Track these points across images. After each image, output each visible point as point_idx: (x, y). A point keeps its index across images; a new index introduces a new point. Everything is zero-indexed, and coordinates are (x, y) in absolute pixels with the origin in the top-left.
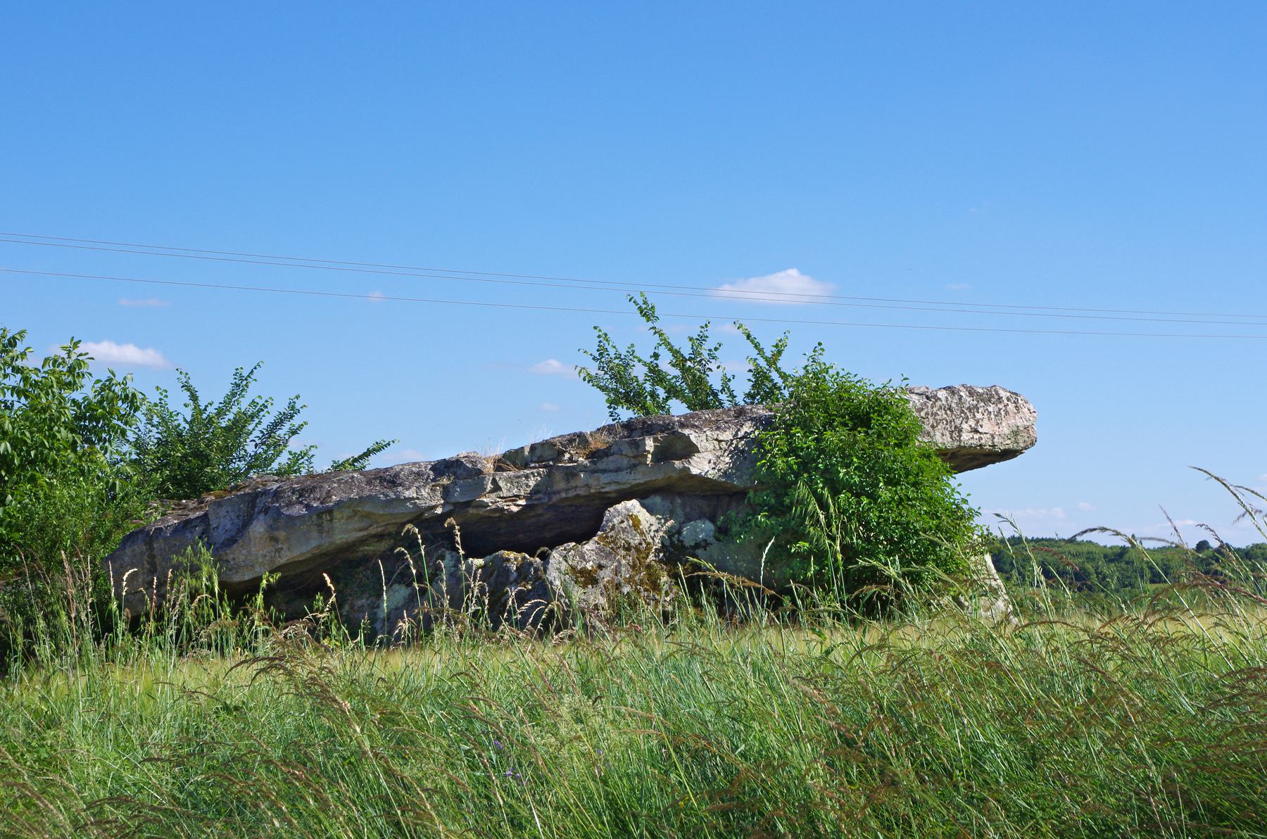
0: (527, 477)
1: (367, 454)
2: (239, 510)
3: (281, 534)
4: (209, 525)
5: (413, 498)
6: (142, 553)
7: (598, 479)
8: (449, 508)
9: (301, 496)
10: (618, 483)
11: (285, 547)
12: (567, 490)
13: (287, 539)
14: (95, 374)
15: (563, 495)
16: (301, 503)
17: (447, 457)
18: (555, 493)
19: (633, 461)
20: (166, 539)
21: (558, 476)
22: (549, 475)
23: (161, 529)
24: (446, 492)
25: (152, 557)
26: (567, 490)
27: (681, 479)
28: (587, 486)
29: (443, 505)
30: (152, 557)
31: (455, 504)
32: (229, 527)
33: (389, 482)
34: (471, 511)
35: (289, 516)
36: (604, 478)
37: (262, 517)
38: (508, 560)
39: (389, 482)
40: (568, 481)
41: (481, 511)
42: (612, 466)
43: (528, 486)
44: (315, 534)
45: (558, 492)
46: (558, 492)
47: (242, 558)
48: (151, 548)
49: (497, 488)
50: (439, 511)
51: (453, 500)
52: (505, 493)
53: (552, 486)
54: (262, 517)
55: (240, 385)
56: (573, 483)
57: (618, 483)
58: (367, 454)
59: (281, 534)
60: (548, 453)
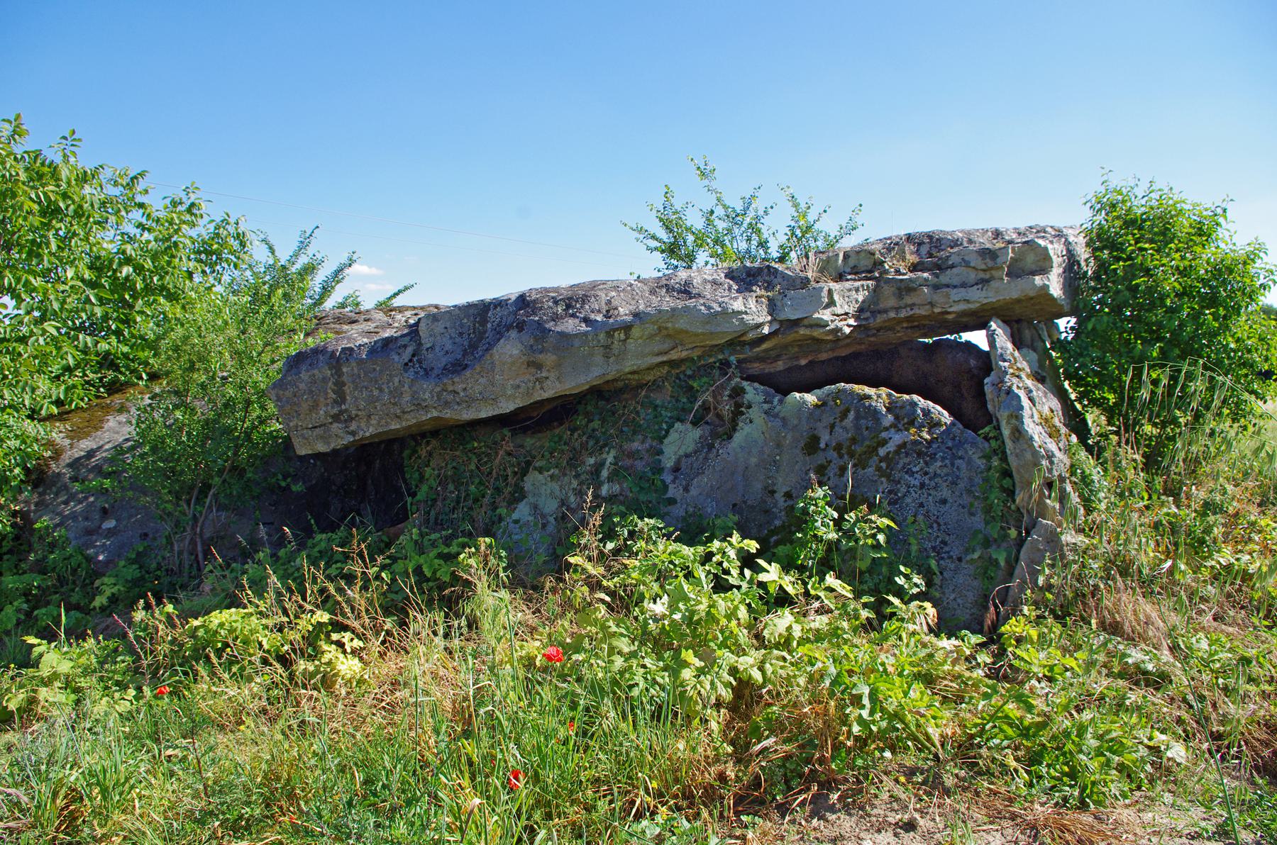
0: (857, 290)
1: (396, 295)
2: (462, 326)
3: (549, 359)
4: (420, 344)
5: (740, 313)
6: (325, 380)
7: (948, 296)
8: (776, 326)
9: (568, 306)
10: (968, 301)
11: (552, 375)
12: (897, 309)
13: (558, 365)
14: (212, 211)
15: (892, 315)
16: (573, 316)
17: (470, 300)
18: (879, 312)
19: (982, 275)
20: (361, 362)
21: (887, 290)
22: (876, 291)
23: (351, 349)
24: (772, 307)
25: (340, 385)
26: (897, 309)
27: (1038, 296)
28: (932, 304)
29: (770, 322)
30: (340, 385)
31: (781, 322)
32: (449, 347)
33: (680, 292)
34: (802, 331)
35: (563, 335)
36: (955, 294)
37: (513, 334)
38: (869, 397)
39: (680, 292)
40: (900, 297)
41: (816, 333)
42: (955, 281)
43: (857, 301)
44: (598, 358)
45: (886, 311)
46: (886, 311)
47: (478, 388)
48: (339, 373)
49: (832, 303)
50: (766, 330)
51: (782, 317)
52: (839, 310)
53: (876, 303)
54: (513, 334)
55: (303, 246)
56: (908, 300)
57: (968, 301)
58: (396, 295)
59: (549, 359)
60: (865, 263)
